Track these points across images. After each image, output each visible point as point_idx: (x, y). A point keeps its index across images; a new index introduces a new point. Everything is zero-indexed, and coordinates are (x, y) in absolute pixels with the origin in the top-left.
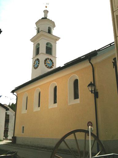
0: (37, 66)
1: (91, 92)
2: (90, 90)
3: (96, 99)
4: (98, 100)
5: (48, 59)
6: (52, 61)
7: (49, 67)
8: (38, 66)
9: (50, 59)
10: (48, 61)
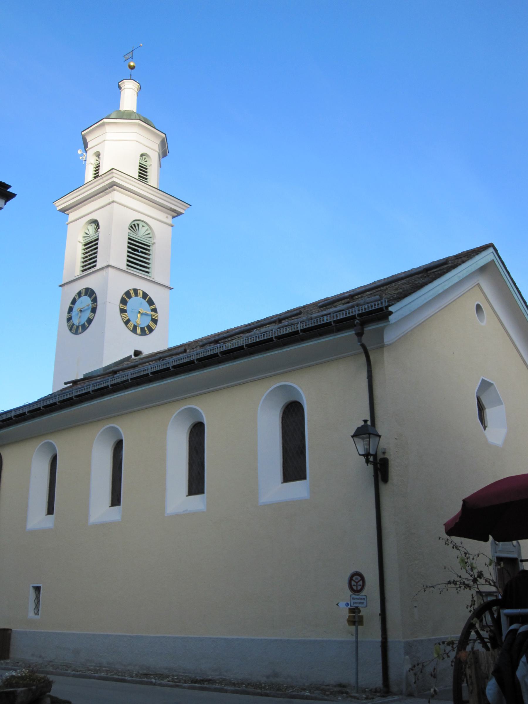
0: (84, 320)
1: (363, 459)
2: (362, 452)
3: (382, 486)
4: (383, 488)
5: (136, 291)
6: (151, 302)
7: (139, 330)
8: (90, 321)
9: (145, 295)
10: (135, 302)
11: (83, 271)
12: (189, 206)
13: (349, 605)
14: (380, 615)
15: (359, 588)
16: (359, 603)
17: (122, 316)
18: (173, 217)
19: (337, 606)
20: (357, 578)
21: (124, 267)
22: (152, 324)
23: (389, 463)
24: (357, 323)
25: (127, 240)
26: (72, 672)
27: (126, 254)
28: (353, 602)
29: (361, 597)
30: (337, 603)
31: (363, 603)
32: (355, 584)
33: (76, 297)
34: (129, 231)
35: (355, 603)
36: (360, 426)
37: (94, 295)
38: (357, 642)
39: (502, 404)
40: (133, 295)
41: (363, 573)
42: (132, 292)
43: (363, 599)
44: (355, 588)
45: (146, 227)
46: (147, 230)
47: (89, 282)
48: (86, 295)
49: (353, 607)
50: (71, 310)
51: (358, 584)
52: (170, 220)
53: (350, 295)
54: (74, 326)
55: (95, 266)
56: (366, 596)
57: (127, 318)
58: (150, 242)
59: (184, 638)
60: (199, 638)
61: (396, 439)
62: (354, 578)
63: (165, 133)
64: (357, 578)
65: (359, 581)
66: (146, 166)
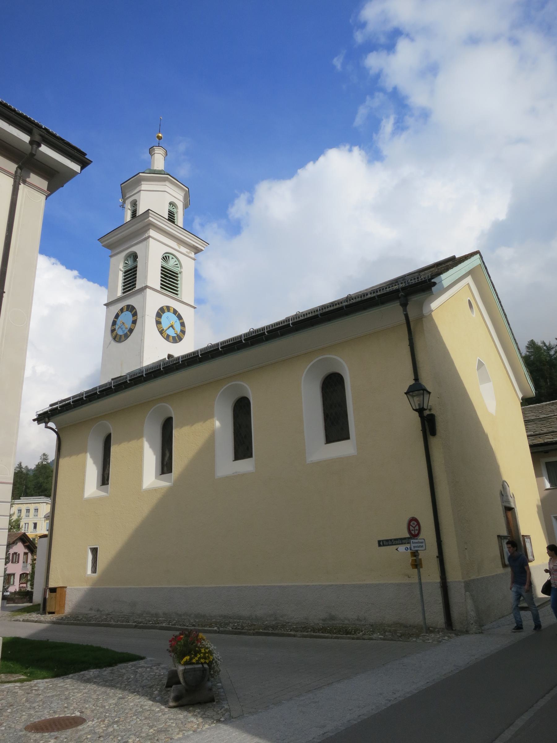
5: (168, 308)
6: (180, 317)
7: (171, 339)
8: (131, 331)
9: (175, 312)
11: (124, 293)
12: (207, 245)
13: (408, 549)
14: (437, 557)
15: (417, 532)
16: (419, 547)
17: (158, 326)
18: (195, 253)
19: (396, 551)
20: (413, 523)
21: (159, 289)
22: (181, 335)
23: (436, 418)
24: (402, 295)
25: (160, 268)
26: (134, 624)
27: (160, 278)
28: (414, 546)
29: (420, 541)
30: (396, 548)
31: (422, 546)
32: (413, 529)
33: (119, 313)
34: (162, 261)
35: (415, 546)
36: (412, 384)
37: (135, 310)
38: (420, 583)
39: (491, 382)
40: (166, 311)
41: (418, 519)
42: (165, 308)
43: (422, 542)
44: (413, 532)
45: (175, 259)
46: (176, 261)
47: (130, 302)
48: (127, 310)
49: (413, 550)
50: (114, 323)
51: (415, 528)
52: (192, 255)
53: (142, 459)
54: (118, 335)
55: (135, 287)
56: (424, 539)
57: (162, 328)
58: (178, 271)
59: (238, 587)
60: (253, 586)
61: (438, 398)
62: (411, 524)
63: (188, 187)
64: (414, 524)
65: (416, 526)
66: (174, 212)
